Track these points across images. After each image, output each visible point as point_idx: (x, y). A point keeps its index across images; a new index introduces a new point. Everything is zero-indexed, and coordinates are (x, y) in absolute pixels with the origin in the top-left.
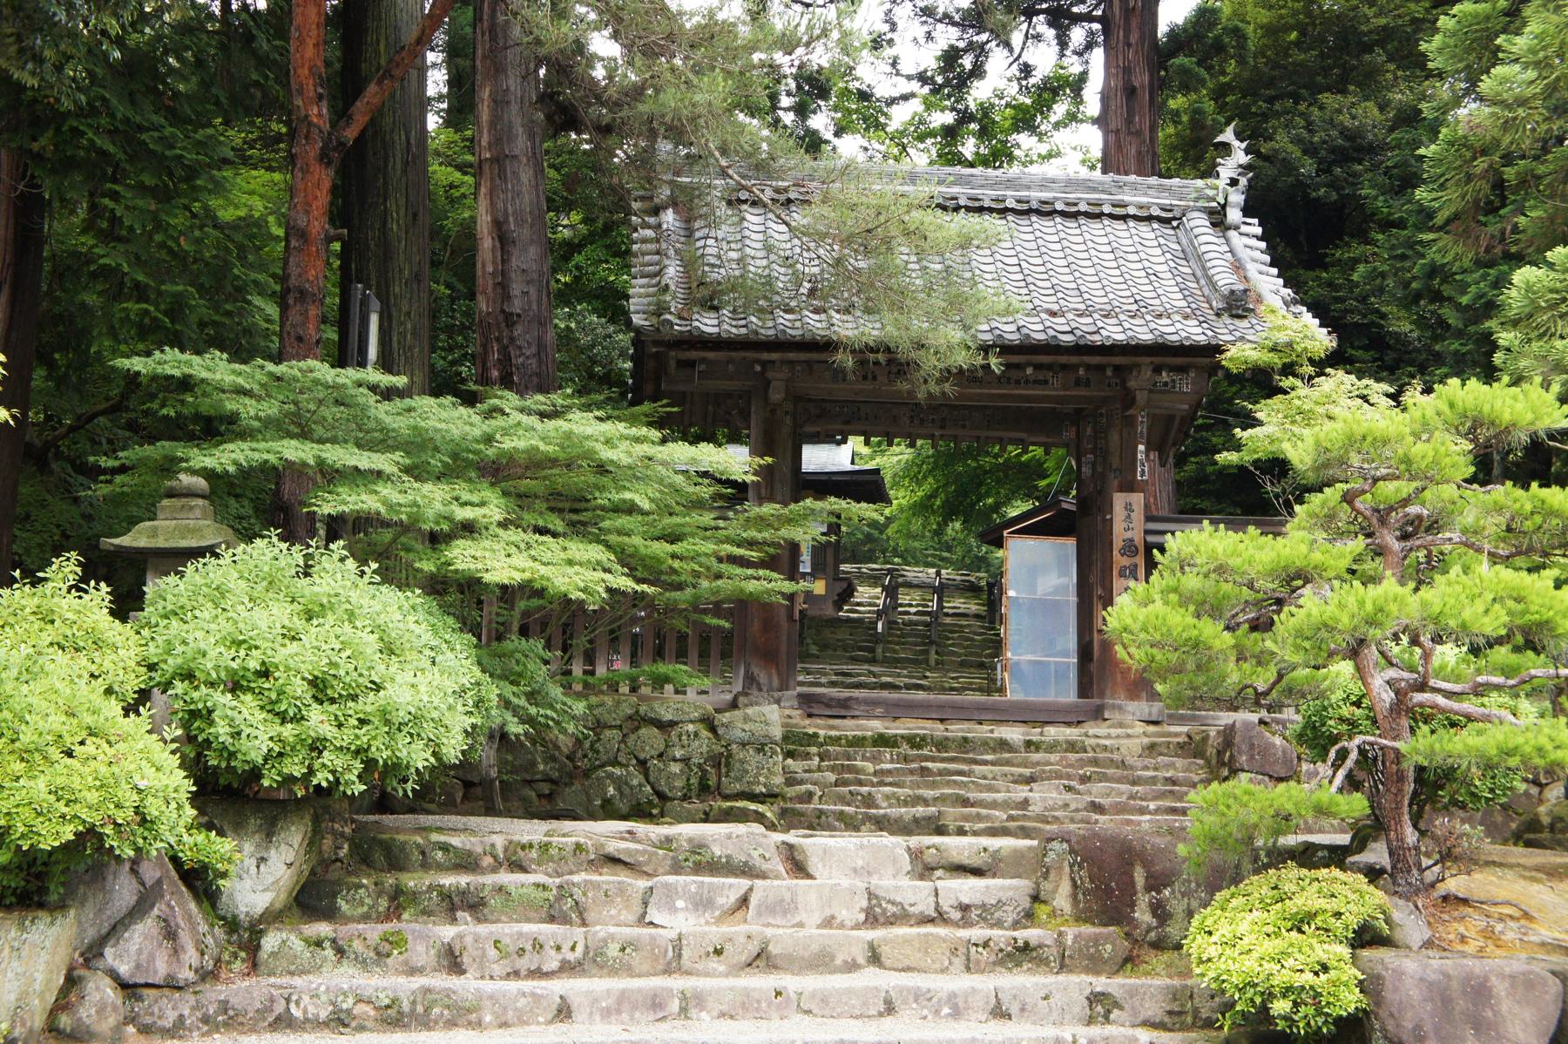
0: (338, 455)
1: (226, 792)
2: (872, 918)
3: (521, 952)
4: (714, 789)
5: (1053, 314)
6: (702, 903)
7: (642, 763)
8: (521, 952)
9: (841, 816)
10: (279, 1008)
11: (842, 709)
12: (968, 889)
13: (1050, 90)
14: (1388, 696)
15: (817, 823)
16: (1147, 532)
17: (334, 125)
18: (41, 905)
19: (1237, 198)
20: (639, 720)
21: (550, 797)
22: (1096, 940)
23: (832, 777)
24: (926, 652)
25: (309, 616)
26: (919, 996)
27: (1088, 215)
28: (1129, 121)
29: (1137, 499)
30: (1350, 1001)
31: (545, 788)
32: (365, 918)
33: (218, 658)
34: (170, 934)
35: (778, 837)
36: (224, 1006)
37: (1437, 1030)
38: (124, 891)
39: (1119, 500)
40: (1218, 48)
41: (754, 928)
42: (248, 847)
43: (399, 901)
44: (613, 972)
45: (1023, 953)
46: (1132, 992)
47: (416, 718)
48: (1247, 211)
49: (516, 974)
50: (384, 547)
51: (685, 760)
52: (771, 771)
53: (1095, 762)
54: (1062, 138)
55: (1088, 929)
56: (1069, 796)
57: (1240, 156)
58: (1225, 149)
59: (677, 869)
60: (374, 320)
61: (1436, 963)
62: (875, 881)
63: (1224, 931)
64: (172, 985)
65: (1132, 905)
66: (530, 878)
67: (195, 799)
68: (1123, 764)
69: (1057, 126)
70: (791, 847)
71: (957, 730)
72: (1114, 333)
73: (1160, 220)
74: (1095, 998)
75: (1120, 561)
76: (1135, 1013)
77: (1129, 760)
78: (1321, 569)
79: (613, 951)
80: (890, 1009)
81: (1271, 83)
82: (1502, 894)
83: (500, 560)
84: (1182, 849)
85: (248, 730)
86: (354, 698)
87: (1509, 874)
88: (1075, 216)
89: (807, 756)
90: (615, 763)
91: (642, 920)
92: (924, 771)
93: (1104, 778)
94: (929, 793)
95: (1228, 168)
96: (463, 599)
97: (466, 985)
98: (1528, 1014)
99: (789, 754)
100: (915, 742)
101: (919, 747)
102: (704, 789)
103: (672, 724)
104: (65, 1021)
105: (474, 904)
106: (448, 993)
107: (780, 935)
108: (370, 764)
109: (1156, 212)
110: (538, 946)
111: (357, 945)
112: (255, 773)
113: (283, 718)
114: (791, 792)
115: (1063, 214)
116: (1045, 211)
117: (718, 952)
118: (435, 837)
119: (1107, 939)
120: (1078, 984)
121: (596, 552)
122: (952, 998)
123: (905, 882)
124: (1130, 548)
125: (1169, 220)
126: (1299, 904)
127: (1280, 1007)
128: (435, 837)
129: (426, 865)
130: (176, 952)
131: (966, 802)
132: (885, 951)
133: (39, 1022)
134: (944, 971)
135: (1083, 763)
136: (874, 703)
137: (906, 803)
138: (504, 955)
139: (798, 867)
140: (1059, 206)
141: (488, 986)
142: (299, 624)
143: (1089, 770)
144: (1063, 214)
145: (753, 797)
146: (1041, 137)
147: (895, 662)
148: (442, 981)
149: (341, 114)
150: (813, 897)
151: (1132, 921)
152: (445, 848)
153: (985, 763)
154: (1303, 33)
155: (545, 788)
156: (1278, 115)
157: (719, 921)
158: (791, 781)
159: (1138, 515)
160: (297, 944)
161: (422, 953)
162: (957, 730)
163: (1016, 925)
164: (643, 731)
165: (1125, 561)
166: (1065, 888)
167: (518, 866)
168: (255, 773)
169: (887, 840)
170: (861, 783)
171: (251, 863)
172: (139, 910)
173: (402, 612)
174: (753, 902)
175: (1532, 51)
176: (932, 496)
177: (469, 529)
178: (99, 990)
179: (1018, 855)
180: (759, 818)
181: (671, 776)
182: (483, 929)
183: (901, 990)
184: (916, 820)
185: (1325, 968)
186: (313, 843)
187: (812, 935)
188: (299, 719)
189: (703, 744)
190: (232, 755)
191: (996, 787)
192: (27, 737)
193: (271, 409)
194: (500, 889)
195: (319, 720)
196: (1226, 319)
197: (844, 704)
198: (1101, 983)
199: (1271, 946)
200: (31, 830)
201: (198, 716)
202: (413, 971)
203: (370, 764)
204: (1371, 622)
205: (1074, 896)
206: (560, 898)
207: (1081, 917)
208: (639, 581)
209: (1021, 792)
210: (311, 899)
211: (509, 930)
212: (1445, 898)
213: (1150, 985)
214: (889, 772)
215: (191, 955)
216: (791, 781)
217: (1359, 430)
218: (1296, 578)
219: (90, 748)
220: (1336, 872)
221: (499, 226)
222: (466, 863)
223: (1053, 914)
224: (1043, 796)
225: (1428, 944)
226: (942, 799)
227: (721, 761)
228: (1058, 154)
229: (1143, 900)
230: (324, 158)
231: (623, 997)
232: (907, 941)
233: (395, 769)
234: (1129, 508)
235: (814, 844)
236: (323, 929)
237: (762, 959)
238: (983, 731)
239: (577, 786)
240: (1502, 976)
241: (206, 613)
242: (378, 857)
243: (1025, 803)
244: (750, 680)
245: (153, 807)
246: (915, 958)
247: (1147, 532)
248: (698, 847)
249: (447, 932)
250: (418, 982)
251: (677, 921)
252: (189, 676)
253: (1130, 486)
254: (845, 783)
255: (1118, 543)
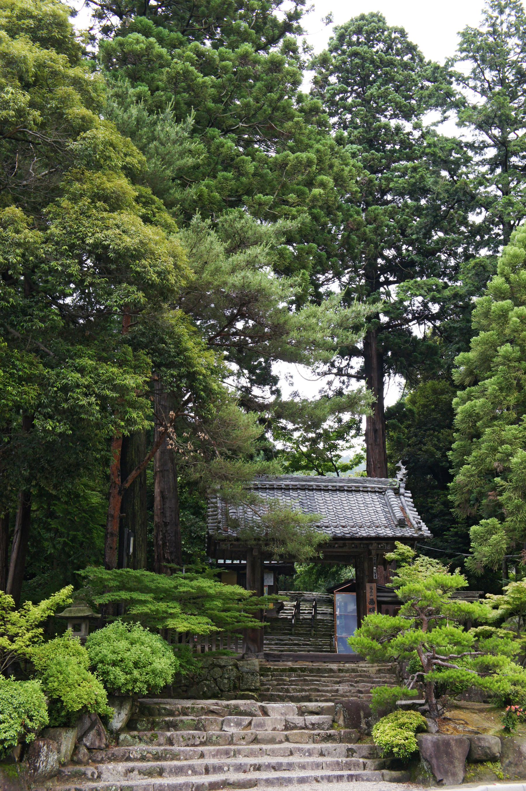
0: (136, 595)
1: (115, 695)
2: (287, 728)
3: (189, 739)
4: (238, 688)
5: (343, 527)
6: (238, 724)
7: (215, 679)
8: (189, 739)
9: (279, 696)
10: (127, 755)
11: (277, 658)
12: (314, 719)
13: (349, 427)
14: (426, 661)
15: (272, 699)
16: (378, 596)
17: (122, 482)
18: (69, 727)
19: (403, 485)
20: (214, 665)
21: (186, 691)
22: (350, 733)
23: (275, 683)
24: (310, 631)
25: (132, 644)
26: (300, 750)
27: (355, 491)
28: (375, 441)
29: (374, 585)
30: (414, 747)
31: (184, 688)
32: (145, 730)
33: (111, 657)
34: (99, 734)
35: (259, 704)
36: (113, 755)
37: (435, 755)
38: (87, 723)
39: (368, 586)
40: (405, 415)
41: (253, 731)
42: (116, 710)
43: (154, 725)
44: (214, 745)
45: (329, 738)
46: (359, 748)
47: (161, 672)
48: (406, 488)
49: (187, 745)
50: (152, 623)
51: (229, 678)
52: (257, 681)
53: (360, 676)
54: (354, 441)
55: (348, 730)
56: (351, 688)
57: (404, 471)
58: (399, 469)
59: (230, 714)
60: (132, 539)
61: (436, 736)
62: (287, 717)
63: (382, 729)
64: (100, 749)
65: (360, 722)
66: (190, 718)
67: (108, 697)
68: (369, 677)
69: (352, 437)
70: (263, 707)
71: (316, 665)
72: (363, 533)
73: (378, 492)
74: (349, 750)
75: (369, 606)
76: (360, 754)
77: (372, 675)
78: (403, 627)
79: (214, 738)
80: (291, 754)
81: (425, 425)
82: (462, 717)
83: (181, 625)
84: (371, 706)
85: (119, 676)
86: (144, 667)
87: (467, 711)
88: (351, 491)
89: (268, 676)
90: (207, 680)
91: (221, 730)
92: (305, 680)
93: (363, 681)
94: (307, 688)
95: (400, 475)
96: (169, 636)
97: (176, 748)
98: (460, 750)
99: (261, 675)
100: (303, 670)
101: (304, 671)
102: (235, 688)
103: (224, 666)
104: (75, 758)
105: (174, 726)
106: (171, 750)
107: (261, 733)
108: (149, 685)
109: (377, 490)
110: (194, 737)
111: (145, 737)
112: (119, 689)
113: (127, 673)
114: (262, 688)
115: (347, 491)
116: (341, 490)
117: (243, 738)
118: (162, 706)
119: (353, 733)
120: (343, 747)
121: (205, 620)
122: (309, 750)
123: (296, 717)
124: (372, 602)
125: (381, 492)
126: (401, 721)
127: (395, 750)
128: (162, 706)
129: (160, 714)
130: (100, 740)
131: (318, 691)
132: (290, 737)
133: (69, 758)
134: (307, 743)
135: (356, 676)
136: (290, 656)
137: (299, 691)
138: (184, 740)
139: (265, 713)
140: (346, 488)
141: (182, 748)
142: (130, 646)
143: (358, 679)
144: (347, 491)
145: (251, 690)
146: (347, 441)
147: (298, 635)
148: (168, 747)
149: (124, 478)
150: (270, 722)
151: (360, 727)
152: (165, 709)
153: (325, 677)
154: (436, 405)
155: (184, 688)
156: (428, 436)
157: (243, 729)
158: (262, 684)
159: (374, 591)
160: (129, 737)
161: (162, 740)
162: (316, 665)
163: (328, 729)
164: (215, 669)
165: (371, 606)
166: (342, 718)
167: (186, 715)
168: (119, 689)
169: (292, 704)
170: (285, 685)
171: (116, 714)
172: (91, 728)
173: (155, 641)
174: (253, 723)
175: (474, 461)
176: (312, 568)
177: (173, 616)
178: (83, 750)
179: (329, 708)
180: (252, 698)
181: (224, 684)
182: (178, 732)
183: (294, 748)
184: (302, 697)
185: (407, 739)
186: (131, 708)
187: (269, 733)
188: (131, 673)
189: (234, 673)
190: (114, 684)
191: (329, 686)
192: (70, 681)
193: (116, 583)
194: (182, 721)
195: (136, 673)
196: (399, 528)
197: (279, 656)
198: (350, 746)
199: (393, 733)
200: (72, 706)
201: (106, 673)
202: (160, 745)
203: (149, 685)
204: (415, 642)
205: (344, 720)
206: (198, 723)
207: (346, 727)
208: (219, 627)
209: (336, 687)
210: (130, 725)
211: (185, 733)
212: (444, 719)
213: (364, 747)
214: (294, 681)
215: (104, 740)
216: (262, 684)
217: (412, 589)
218: (397, 630)
219: (84, 684)
220: (412, 712)
221: (162, 493)
222: (171, 713)
223: (338, 726)
224: (342, 688)
225: (438, 732)
226: (311, 690)
227: (240, 678)
228: (353, 447)
229: (363, 721)
230: (119, 493)
231: (218, 751)
232: (296, 734)
233: (156, 686)
234: (371, 588)
235: (271, 706)
236: (136, 733)
237: (256, 740)
238: (325, 666)
239: (194, 688)
240: (453, 740)
241: (106, 644)
242: (146, 712)
243: (337, 691)
244: (248, 649)
245: (99, 699)
246: (299, 739)
247: (378, 596)
248: (236, 707)
249: (169, 734)
250: (162, 748)
251: (231, 730)
252: (102, 662)
253: (371, 581)
254: (280, 685)
255: (368, 600)
